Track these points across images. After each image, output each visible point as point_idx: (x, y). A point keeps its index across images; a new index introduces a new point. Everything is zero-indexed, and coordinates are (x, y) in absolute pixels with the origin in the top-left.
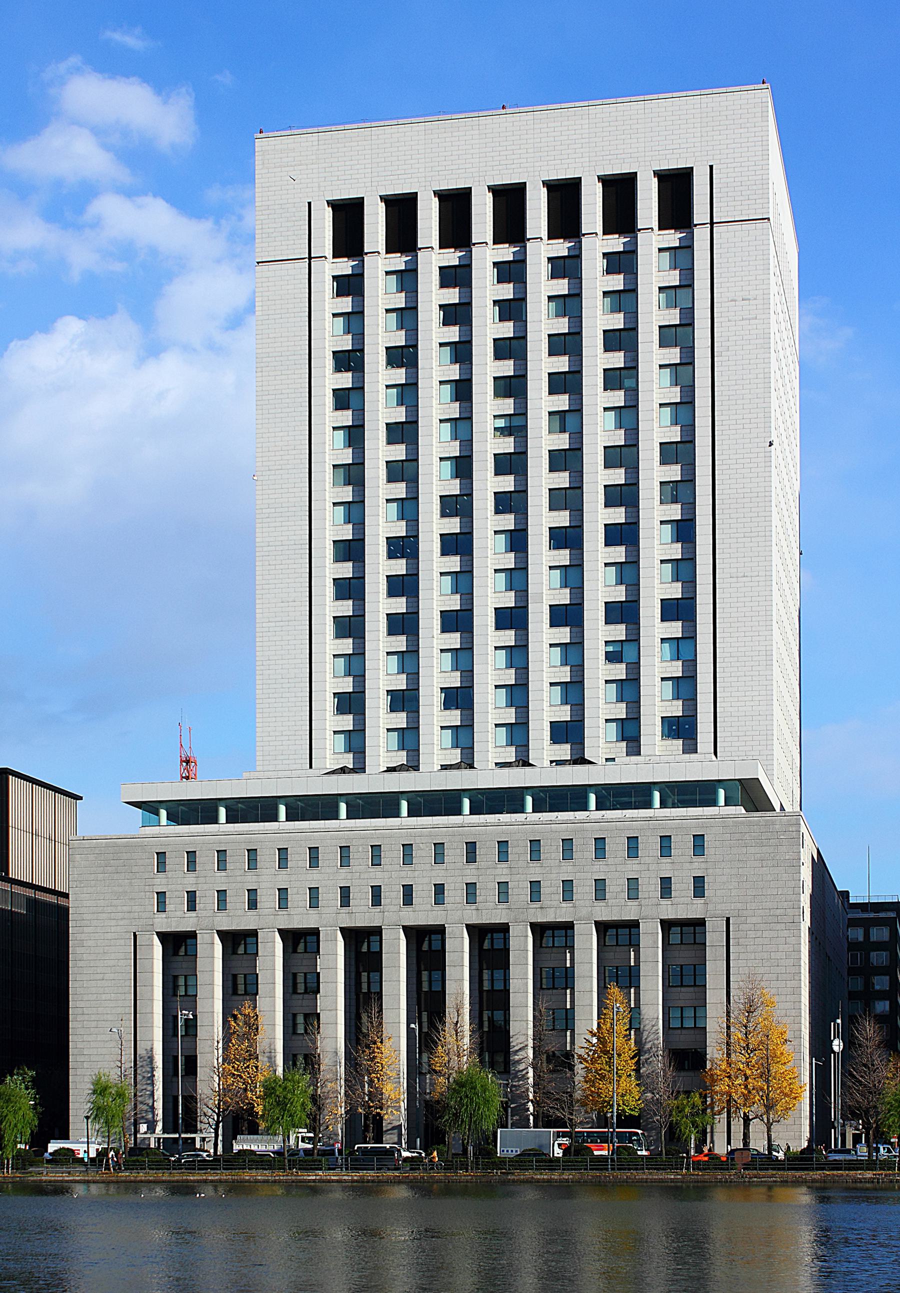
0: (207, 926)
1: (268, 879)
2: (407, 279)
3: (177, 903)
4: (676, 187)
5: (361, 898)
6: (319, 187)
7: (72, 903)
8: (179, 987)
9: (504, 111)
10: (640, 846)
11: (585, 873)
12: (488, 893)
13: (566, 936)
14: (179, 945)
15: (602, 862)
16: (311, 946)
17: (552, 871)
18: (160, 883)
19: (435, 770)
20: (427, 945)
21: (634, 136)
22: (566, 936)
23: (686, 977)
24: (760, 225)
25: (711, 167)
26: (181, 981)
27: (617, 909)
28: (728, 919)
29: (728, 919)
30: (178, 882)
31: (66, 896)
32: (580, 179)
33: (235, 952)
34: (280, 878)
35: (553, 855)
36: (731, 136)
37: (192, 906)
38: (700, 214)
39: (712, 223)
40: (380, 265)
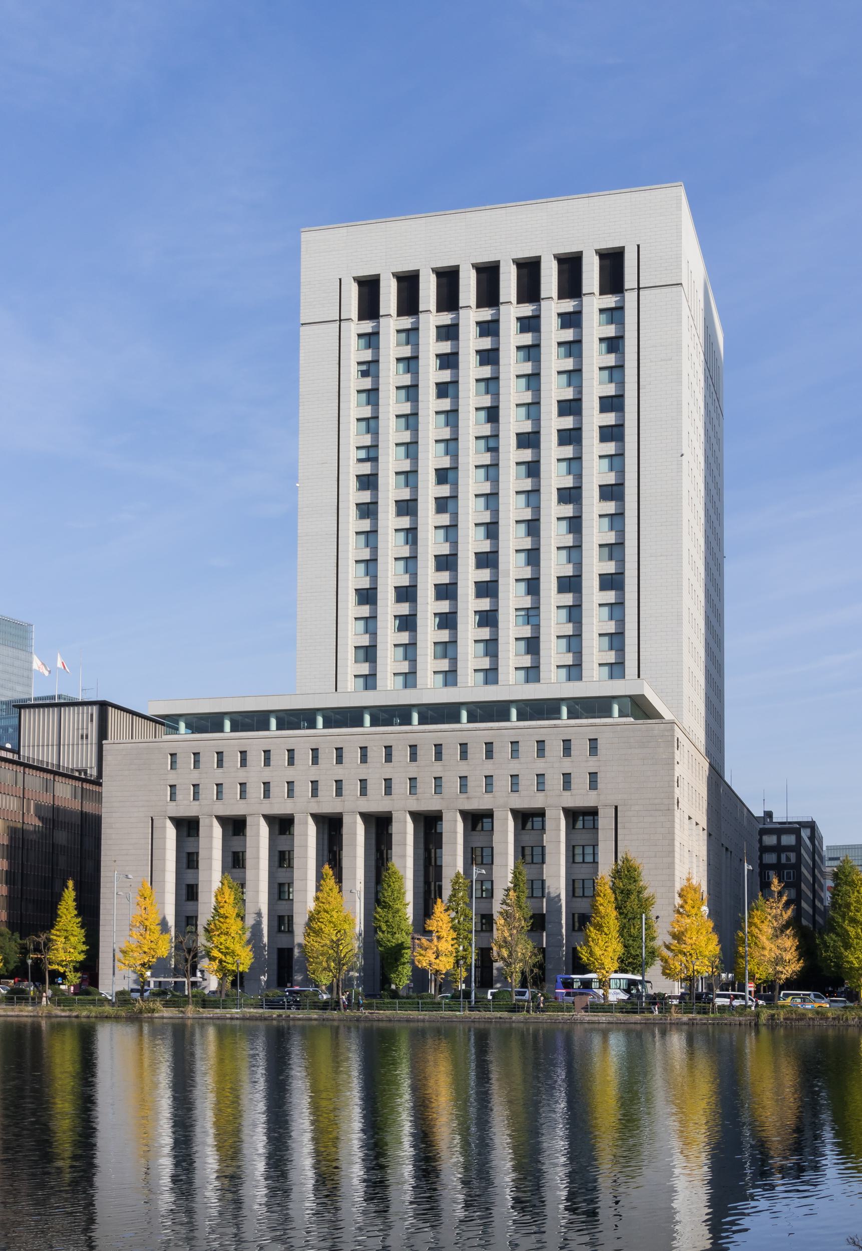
0: (208, 811)
2: (411, 335)
3: (185, 794)
4: (613, 262)
8: (189, 861)
10: (547, 748)
11: (510, 772)
12: (427, 786)
13: (594, 820)
14: (188, 827)
15: (542, 760)
16: (487, 826)
17: (528, 765)
20: (380, 826)
22: (594, 820)
23: (581, 853)
24: (674, 289)
28: (616, 808)
29: (616, 808)
34: (591, 763)
36: (661, 227)
38: (630, 280)
39: (639, 288)
40: (391, 324)
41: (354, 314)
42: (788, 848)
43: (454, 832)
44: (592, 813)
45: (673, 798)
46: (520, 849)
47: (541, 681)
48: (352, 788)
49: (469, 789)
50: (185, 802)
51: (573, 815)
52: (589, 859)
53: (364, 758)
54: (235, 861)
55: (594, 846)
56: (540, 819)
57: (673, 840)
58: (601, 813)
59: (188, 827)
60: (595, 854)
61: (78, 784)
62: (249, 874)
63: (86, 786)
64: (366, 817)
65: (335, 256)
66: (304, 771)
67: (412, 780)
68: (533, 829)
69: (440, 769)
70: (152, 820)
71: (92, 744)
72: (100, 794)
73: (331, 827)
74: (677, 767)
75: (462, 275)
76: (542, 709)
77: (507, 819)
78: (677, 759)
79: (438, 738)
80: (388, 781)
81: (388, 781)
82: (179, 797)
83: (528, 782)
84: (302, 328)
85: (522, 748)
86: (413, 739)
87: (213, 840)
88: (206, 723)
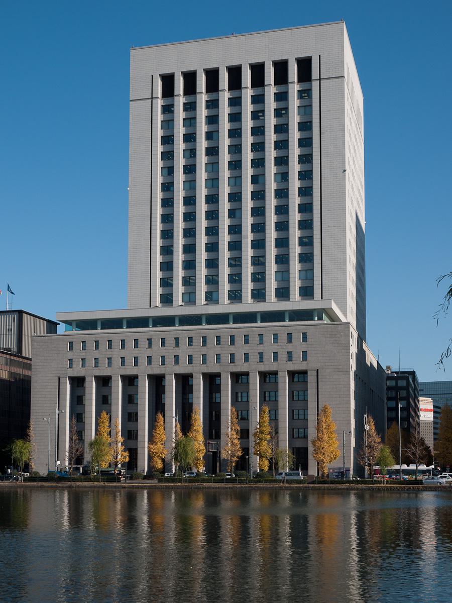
1: (117, 352)
3: (78, 364)
4: (305, 65)
5: (157, 361)
6: (156, 69)
7: (32, 362)
8: (78, 400)
9: (233, 36)
13: (275, 378)
14: (78, 383)
16: (245, 381)
17: (130, 352)
18: (70, 355)
19: (203, 304)
20: (184, 381)
21: (288, 44)
22: (275, 378)
24: (340, 79)
25: (320, 56)
26: (239, 395)
27: (268, 366)
29: (318, 370)
30: (78, 354)
31: (30, 360)
32: (311, 57)
33: (265, 381)
35: (240, 342)
37: (191, 362)
38: (315, 75)
39: (320, 79)
41: (160, 95)
42: (402, 388)
44: (304, 373)
46: (263, 393)
47: (267, 301)
48: (254, 358)
50: (130, 367)
51: (264, 375)
52: (301, 398)
53: (177, 344)
54: (104, 401)
55: (275, 392)
56: (246, 377)
57: (350, 388)
60: (276, 396)
61: (8, 357)
62: (113, 408)
63: (12, 358)
65: (148, 64)
69: (219, 349)
71: (14, 334)
72: (30, 365)
75: (220, 72)
76: (194, 320)
77: (92, 382)
78: (351, 343)
79: (218, 333)
82: (74, 366)
84: (131, 103)
87: (92, 389)
88: (89, 324)
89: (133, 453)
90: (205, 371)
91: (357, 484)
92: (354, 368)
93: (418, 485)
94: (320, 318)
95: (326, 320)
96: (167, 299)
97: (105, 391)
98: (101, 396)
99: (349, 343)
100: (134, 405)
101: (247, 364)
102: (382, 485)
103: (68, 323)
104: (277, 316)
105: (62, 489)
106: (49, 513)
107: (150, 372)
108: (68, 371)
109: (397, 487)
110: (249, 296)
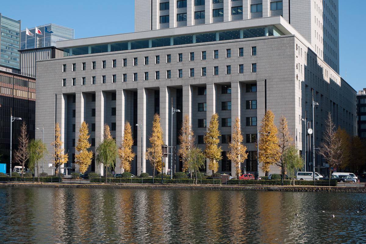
8: (71, 113)
14: (71, 98)
29: (266, 80)
30: (70, 75)
37: (229, 72)
43: (212, 94)
45: (294, 74)
47: (263, 17)
48: (211, 71)
49: (195, 75)
58: (258, 84)
59: (71, 98)
64: (170, 89)
66: (141, 68)
67: (169, 71)
68: (252, 92)
69: (181, 65)
70: (56, 95)
73: (154, 94)
74: (296, 58)
80: (229, 67)
81: (229, 67)
82: (67, 84)
83: (223, 70)
85: (220, 53)
86: (241, 45)
87: (101, 101)
88: (81, 50)
89: (72, 158)
90: (170, 85)
91: (270, 184)
92: (302, 78)
93: (328, 185)
94: (271, 34)
95: (276, 34)
96: (165, 20)
97: (200, 99)
98: (91, 110)
99: (294, 54)
100: (227, 111)
101: (254, 74)
102: (291, 186)
103: (65, 50)
104: (232, 34)
105: (164, 189)
106: (51, 207)
107: (126, 88)
108: (63, 89)
109: (305, 188)
110: (268, 8)
